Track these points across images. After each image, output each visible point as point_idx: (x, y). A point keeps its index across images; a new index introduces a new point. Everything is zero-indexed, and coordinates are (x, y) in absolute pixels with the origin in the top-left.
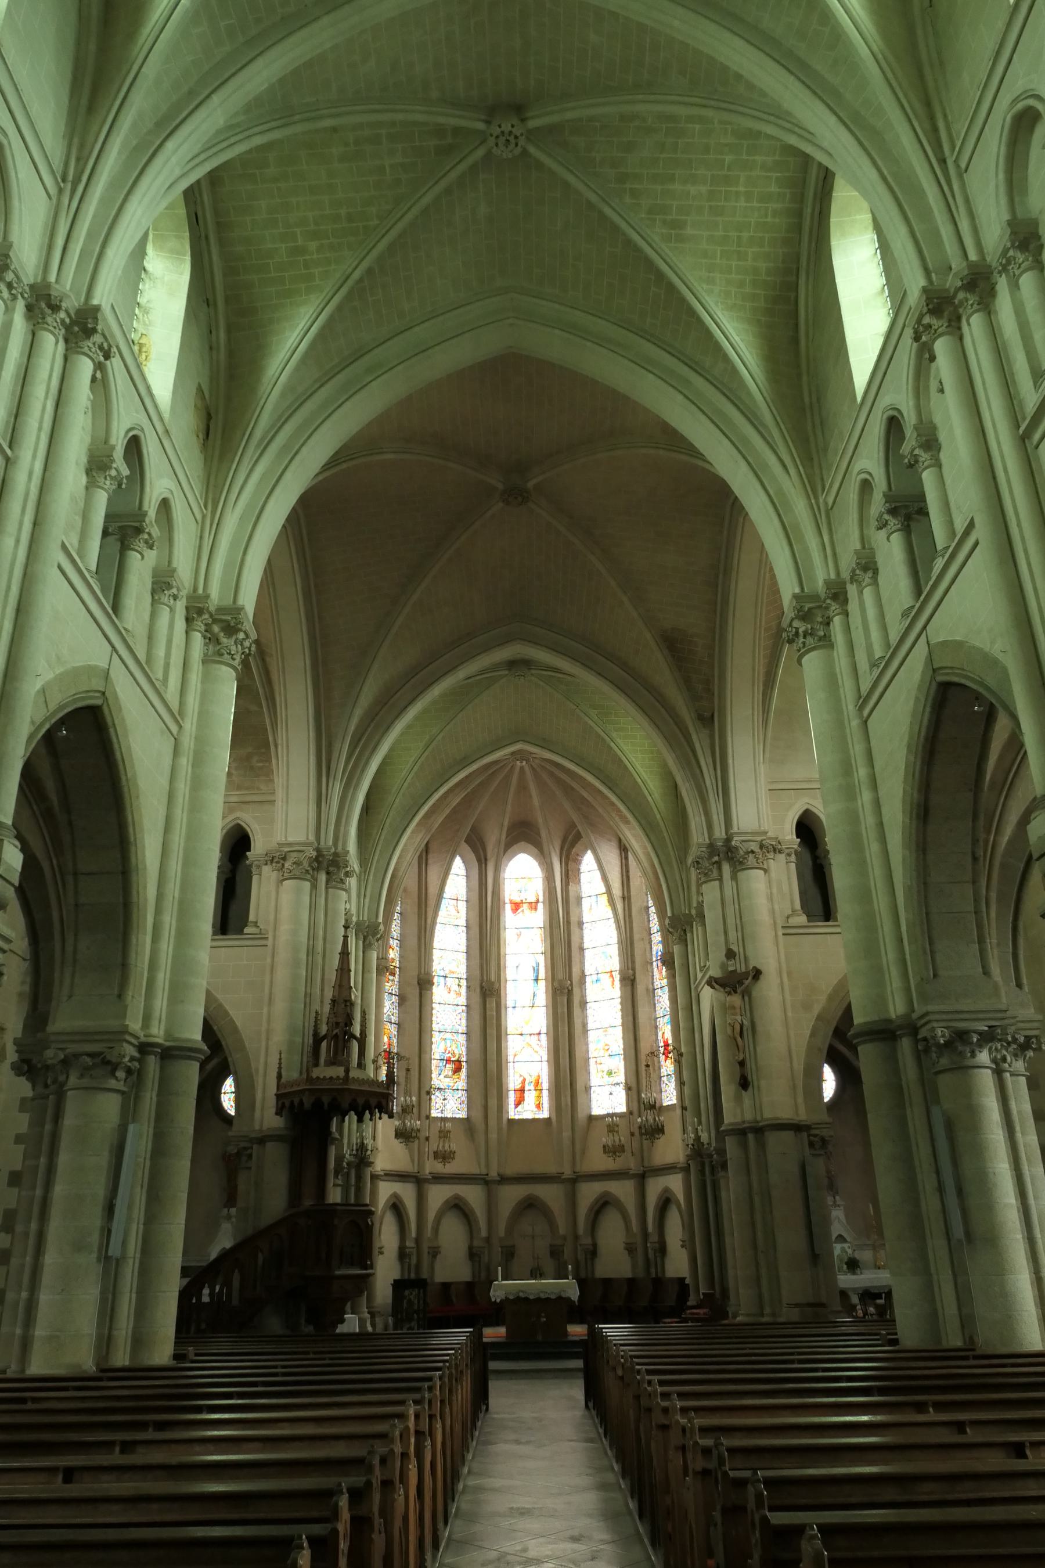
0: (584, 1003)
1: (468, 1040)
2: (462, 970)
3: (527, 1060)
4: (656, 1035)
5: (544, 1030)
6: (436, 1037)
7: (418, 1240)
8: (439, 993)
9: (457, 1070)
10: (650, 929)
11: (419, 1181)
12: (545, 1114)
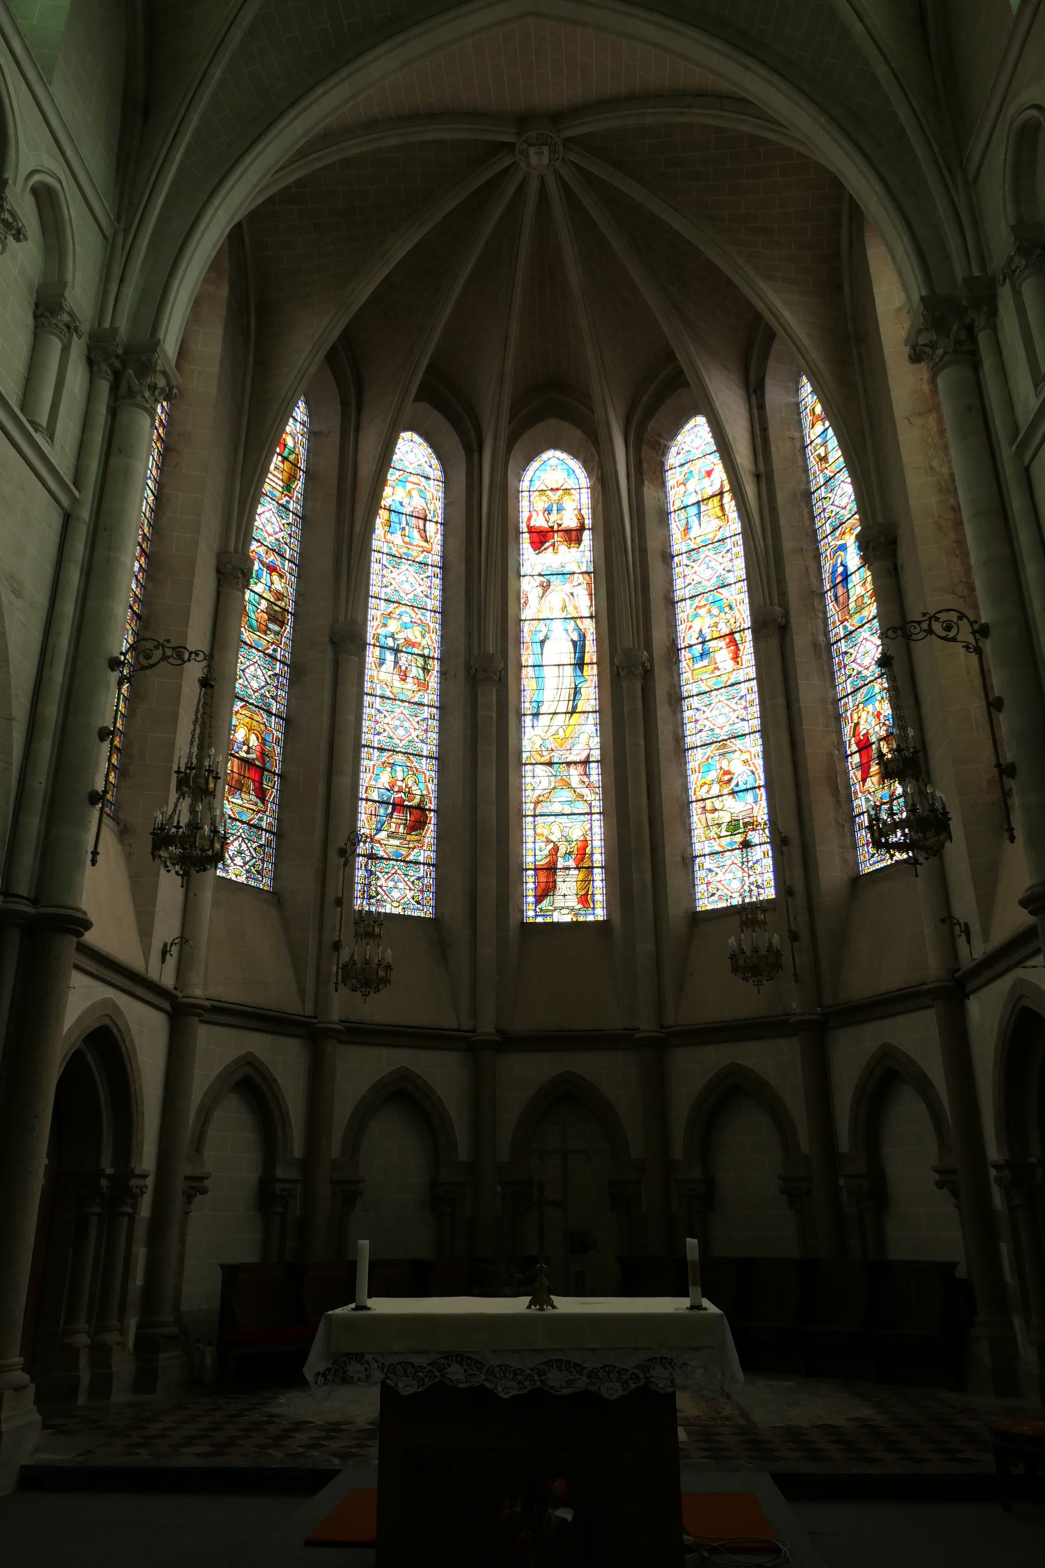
0: (677, 699)
1: (441, 772)
2: (431, 642)
3: (561, 814)
4: (839, 732)
5: (596, 755)
6: (370, 760)
7: (306, 1166)
8: (380, 674)
9: (417, 825)
10: (815, 531)
11: (314, 1035)
12: (599, 914)
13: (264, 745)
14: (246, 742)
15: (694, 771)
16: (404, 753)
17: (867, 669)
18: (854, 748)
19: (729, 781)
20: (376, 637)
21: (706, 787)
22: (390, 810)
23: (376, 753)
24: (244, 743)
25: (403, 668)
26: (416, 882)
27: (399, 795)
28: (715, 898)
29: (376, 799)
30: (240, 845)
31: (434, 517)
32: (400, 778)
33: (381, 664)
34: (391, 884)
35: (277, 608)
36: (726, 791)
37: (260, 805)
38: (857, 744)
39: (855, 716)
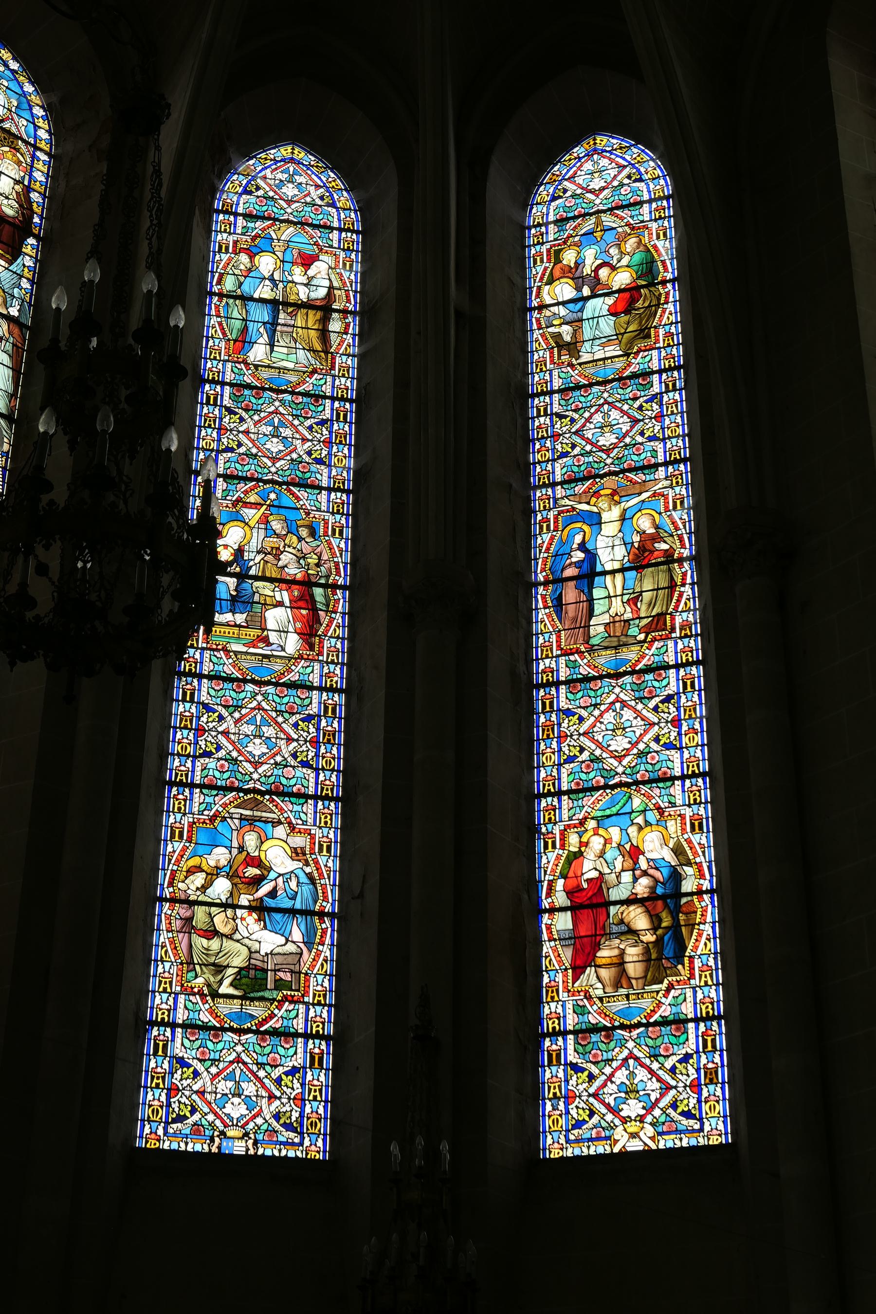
15: (176, 834)
17: (620, 759)
18: (561, 899)
19: (256, 882)
21: (199, 879)
26: (286, 1080)
28: (184, 1128)
36: (244, 900)
38: (569, 893)
39: (573, 840)
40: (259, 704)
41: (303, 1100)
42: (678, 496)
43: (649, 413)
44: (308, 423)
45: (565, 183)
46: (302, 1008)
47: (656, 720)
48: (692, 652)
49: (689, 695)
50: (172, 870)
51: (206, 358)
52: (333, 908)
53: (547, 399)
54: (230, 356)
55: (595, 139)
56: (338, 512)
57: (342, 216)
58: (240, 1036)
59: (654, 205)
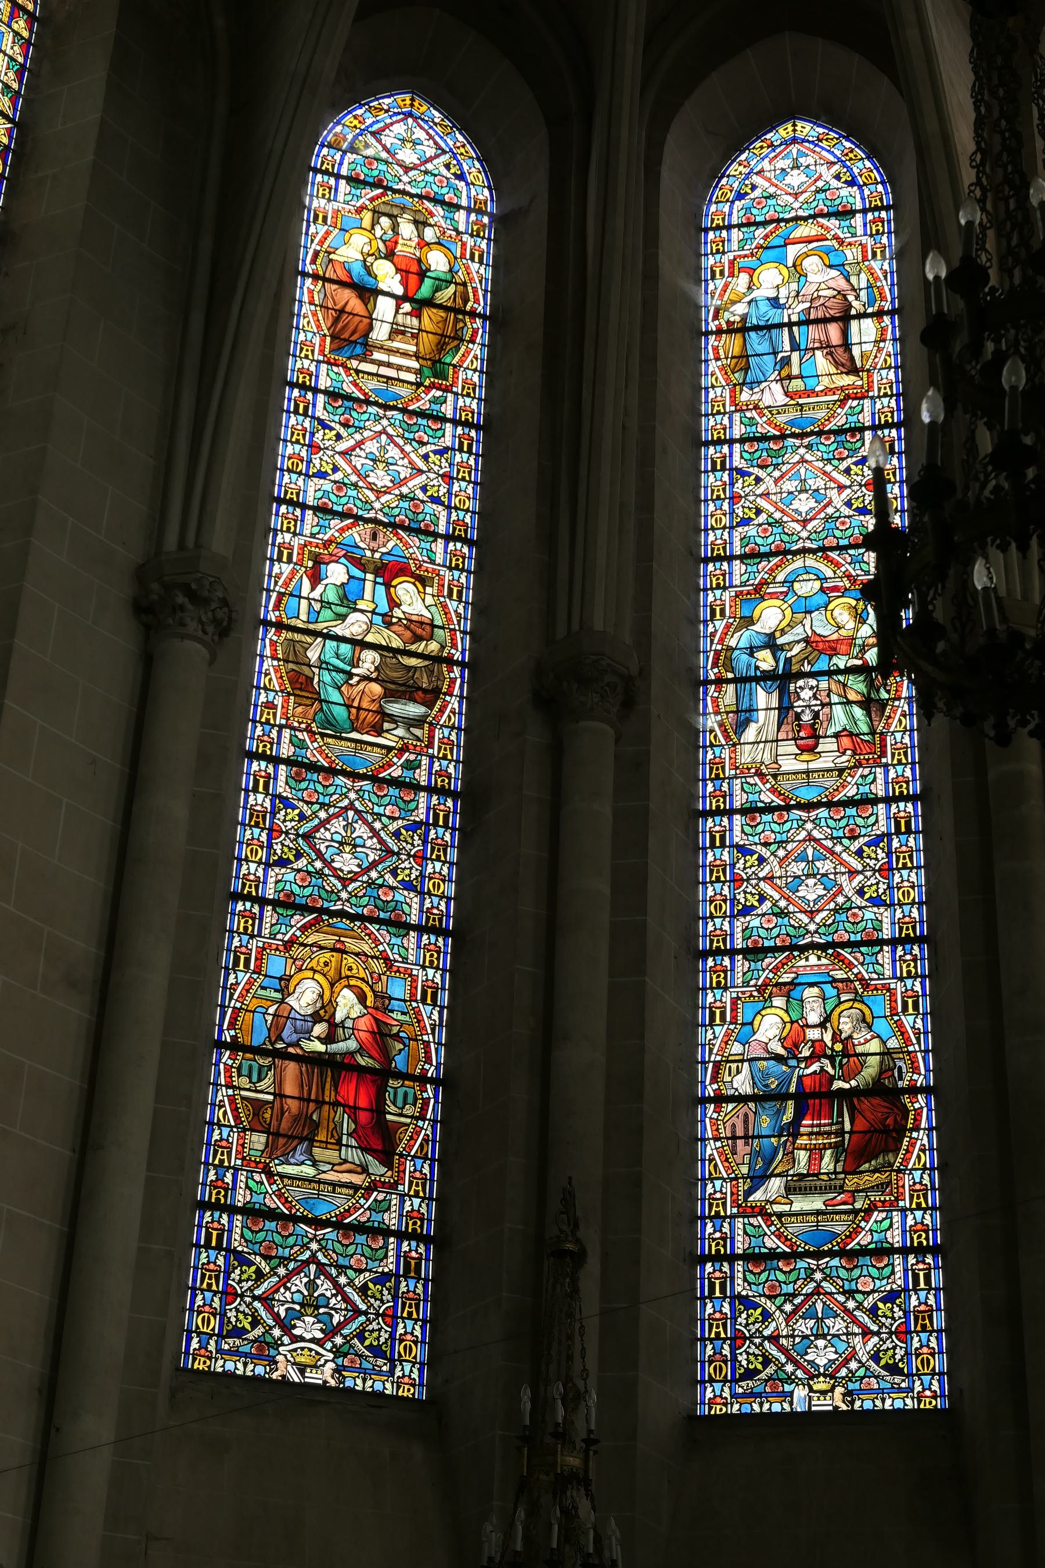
13: (387, 1010)
14: (324, 1012)
16: (823, 947)
20: (725, 657)
22: (788, 1116)
23: (741, 964)
24: (316, 1018)
25: (807, 717)
26: (433, 457)
27: (815, 1067)
29: (746, 1089)
30: (311, 1285)
31: (871, 302)
32: (813, 1018)
33: (741, 726)
34: (805, 1326)
35: (413, 662)
37: (377, 1169)
40: (378, 498)
41: (395, 1317)
42: (910, 993)
43: (872, 863)
44: (423, 450)
45: (754, 177)
46: (450, 397)
47: (860, 868)
48: (926, 1232)
49: (922, 1294)
50: (234, 1008)
51: (254, 721)
52: (438, 1073)
53: (725, 566)
54: (288, 719)
55: (794, 125)
56: (457, 568)
57: (473, 193)
58: (316, 1230)
59: (870, 216)
